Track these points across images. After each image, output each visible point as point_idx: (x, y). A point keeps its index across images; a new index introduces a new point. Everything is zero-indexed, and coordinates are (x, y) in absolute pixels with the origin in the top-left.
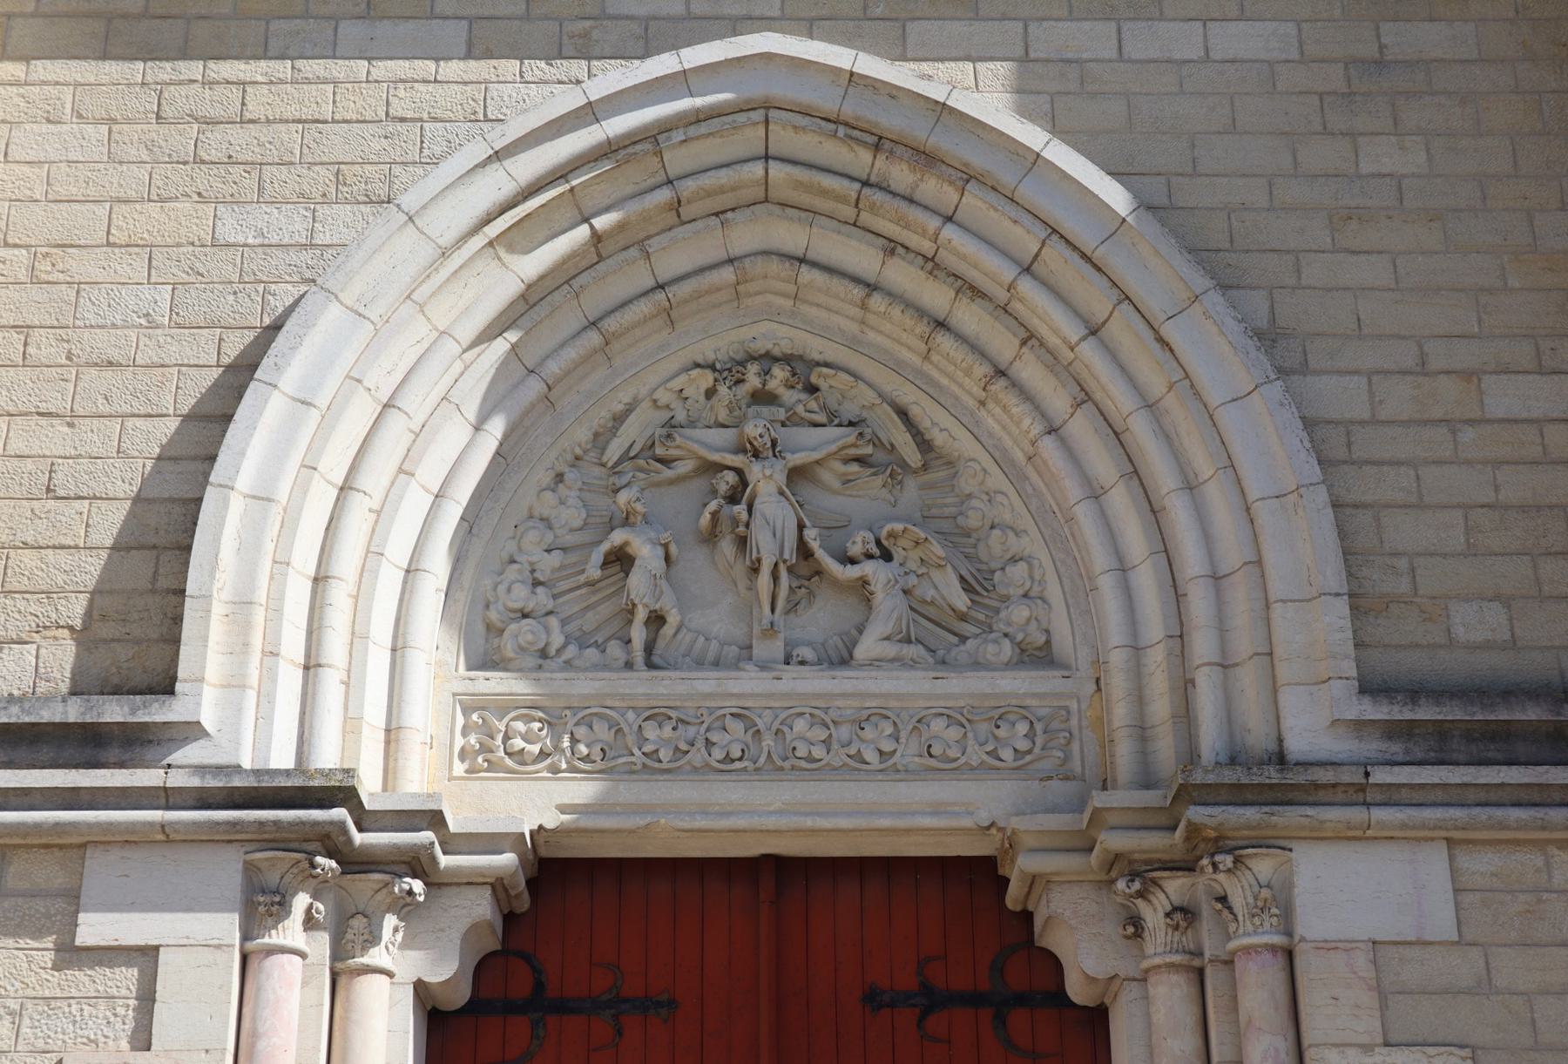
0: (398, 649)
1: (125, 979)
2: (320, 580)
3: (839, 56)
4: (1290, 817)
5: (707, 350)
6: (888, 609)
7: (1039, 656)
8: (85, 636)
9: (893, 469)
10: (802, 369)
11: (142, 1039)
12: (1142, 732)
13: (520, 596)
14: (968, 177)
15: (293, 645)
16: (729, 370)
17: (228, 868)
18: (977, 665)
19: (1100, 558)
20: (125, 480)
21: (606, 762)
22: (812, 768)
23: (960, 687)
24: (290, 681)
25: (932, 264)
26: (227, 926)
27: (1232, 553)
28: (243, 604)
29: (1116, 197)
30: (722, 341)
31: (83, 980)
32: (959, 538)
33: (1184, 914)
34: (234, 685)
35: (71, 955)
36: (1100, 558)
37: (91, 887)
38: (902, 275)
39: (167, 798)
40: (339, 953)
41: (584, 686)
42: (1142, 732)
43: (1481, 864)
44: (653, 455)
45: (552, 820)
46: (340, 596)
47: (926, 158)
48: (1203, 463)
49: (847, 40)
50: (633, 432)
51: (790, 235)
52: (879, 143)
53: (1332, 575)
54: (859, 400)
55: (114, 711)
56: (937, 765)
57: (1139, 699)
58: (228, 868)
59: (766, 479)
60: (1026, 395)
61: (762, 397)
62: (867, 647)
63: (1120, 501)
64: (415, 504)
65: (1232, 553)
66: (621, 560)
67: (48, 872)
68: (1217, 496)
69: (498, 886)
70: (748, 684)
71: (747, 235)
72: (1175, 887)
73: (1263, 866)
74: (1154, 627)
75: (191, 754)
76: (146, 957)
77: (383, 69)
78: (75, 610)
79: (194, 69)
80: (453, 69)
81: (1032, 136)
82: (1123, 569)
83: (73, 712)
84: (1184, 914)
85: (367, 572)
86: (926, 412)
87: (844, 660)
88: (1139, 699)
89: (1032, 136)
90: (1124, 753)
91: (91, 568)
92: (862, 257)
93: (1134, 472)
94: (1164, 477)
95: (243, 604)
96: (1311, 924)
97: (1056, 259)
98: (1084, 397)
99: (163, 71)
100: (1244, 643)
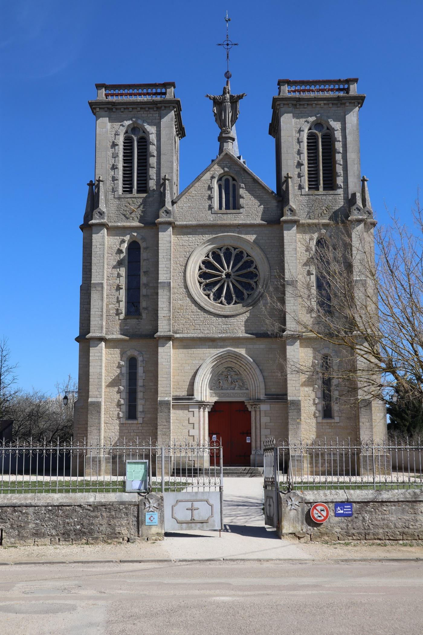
0: (206, 390)
1: (192, 413)
2: (201, 387)
3: (232, 234)
4: (260, 403)
5: (225, 367)
6: (237, 386)
7: (247, 389)
8: (187, 391)
9: (237, 375)
10: (231, 368)
11: (194, 416)
12: (253, 395)
13: (213, 385)
14: (242, 358)
15: (200, 392)
16: (226, 368)
17: (198, 406)
18: (243, 390)
19: (251, 384)
20: (189, 381)
21: (219, 397)
22: (232, 397)
23: (242, 391)
24: (200, 394)
25: (240, 363)
26: (198, 410)
27: (258, 385)
28: (197, 390)
29: (252, 360)
30: (226, 366)
31: (190, 413)
32: (242, 380)
33: (255, 407)
34: (197, 395)
35: (189, 411)
36: (251, 384)
37: (91, 345)
38: (238, 363)
39: (194, 402)
40: (204, 410)
41: (218, 391)
42: (253, 395)
43: (272, 405)
44: (221, 374)
45: (216, 400)
46: (202, 388)
47: (240, 357)
48: (257, 379)
49: (233, 233)
50: (220, 372)
51: (231, 360)
52: (236, 355)
53: (264, 388)
54: (235, 370)
55: (190, 397)
56: (240, 397)
57: (253, 393)
58: (198, 406)
59: (229, 377)
60: (246, 372)
61: (229, 370)
62: (236, 388)
63: (252, 379)
64: (207, 380)
65: (258, 385)
66: (220, 382)
67: (187, 406)
68: (258, 381)
69: (213, 405)
70: (228, 391)
71: (227, 360)
72: (254, 406)
73: (259, 406)
74: (254, 389)
75: (195, 399)
76: (193, 411)
77: (203, 350)
78: (187, 390)
79: (190, 350)
80: (208, 349)
81: (246, 356)
82: (252, 384)
83: (188, 397)
84: (255, 407)
85: (204, 386)
86: (240, 371)
87: (234, 389)
88: (253, 393)
89: (246, 356)
90: (252, 397)
91: (187, 387)
92: (236, 362)
93: (253, 378)
94: (255, 380)
95: (197, 390)
96: (261, 409)
97: (248, 364)
98: (250, 373)
99: (188, 350)
100: (259, 391)
